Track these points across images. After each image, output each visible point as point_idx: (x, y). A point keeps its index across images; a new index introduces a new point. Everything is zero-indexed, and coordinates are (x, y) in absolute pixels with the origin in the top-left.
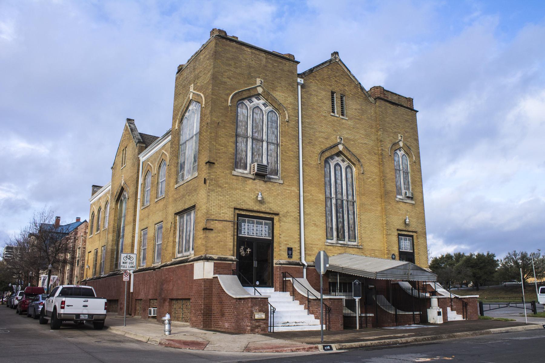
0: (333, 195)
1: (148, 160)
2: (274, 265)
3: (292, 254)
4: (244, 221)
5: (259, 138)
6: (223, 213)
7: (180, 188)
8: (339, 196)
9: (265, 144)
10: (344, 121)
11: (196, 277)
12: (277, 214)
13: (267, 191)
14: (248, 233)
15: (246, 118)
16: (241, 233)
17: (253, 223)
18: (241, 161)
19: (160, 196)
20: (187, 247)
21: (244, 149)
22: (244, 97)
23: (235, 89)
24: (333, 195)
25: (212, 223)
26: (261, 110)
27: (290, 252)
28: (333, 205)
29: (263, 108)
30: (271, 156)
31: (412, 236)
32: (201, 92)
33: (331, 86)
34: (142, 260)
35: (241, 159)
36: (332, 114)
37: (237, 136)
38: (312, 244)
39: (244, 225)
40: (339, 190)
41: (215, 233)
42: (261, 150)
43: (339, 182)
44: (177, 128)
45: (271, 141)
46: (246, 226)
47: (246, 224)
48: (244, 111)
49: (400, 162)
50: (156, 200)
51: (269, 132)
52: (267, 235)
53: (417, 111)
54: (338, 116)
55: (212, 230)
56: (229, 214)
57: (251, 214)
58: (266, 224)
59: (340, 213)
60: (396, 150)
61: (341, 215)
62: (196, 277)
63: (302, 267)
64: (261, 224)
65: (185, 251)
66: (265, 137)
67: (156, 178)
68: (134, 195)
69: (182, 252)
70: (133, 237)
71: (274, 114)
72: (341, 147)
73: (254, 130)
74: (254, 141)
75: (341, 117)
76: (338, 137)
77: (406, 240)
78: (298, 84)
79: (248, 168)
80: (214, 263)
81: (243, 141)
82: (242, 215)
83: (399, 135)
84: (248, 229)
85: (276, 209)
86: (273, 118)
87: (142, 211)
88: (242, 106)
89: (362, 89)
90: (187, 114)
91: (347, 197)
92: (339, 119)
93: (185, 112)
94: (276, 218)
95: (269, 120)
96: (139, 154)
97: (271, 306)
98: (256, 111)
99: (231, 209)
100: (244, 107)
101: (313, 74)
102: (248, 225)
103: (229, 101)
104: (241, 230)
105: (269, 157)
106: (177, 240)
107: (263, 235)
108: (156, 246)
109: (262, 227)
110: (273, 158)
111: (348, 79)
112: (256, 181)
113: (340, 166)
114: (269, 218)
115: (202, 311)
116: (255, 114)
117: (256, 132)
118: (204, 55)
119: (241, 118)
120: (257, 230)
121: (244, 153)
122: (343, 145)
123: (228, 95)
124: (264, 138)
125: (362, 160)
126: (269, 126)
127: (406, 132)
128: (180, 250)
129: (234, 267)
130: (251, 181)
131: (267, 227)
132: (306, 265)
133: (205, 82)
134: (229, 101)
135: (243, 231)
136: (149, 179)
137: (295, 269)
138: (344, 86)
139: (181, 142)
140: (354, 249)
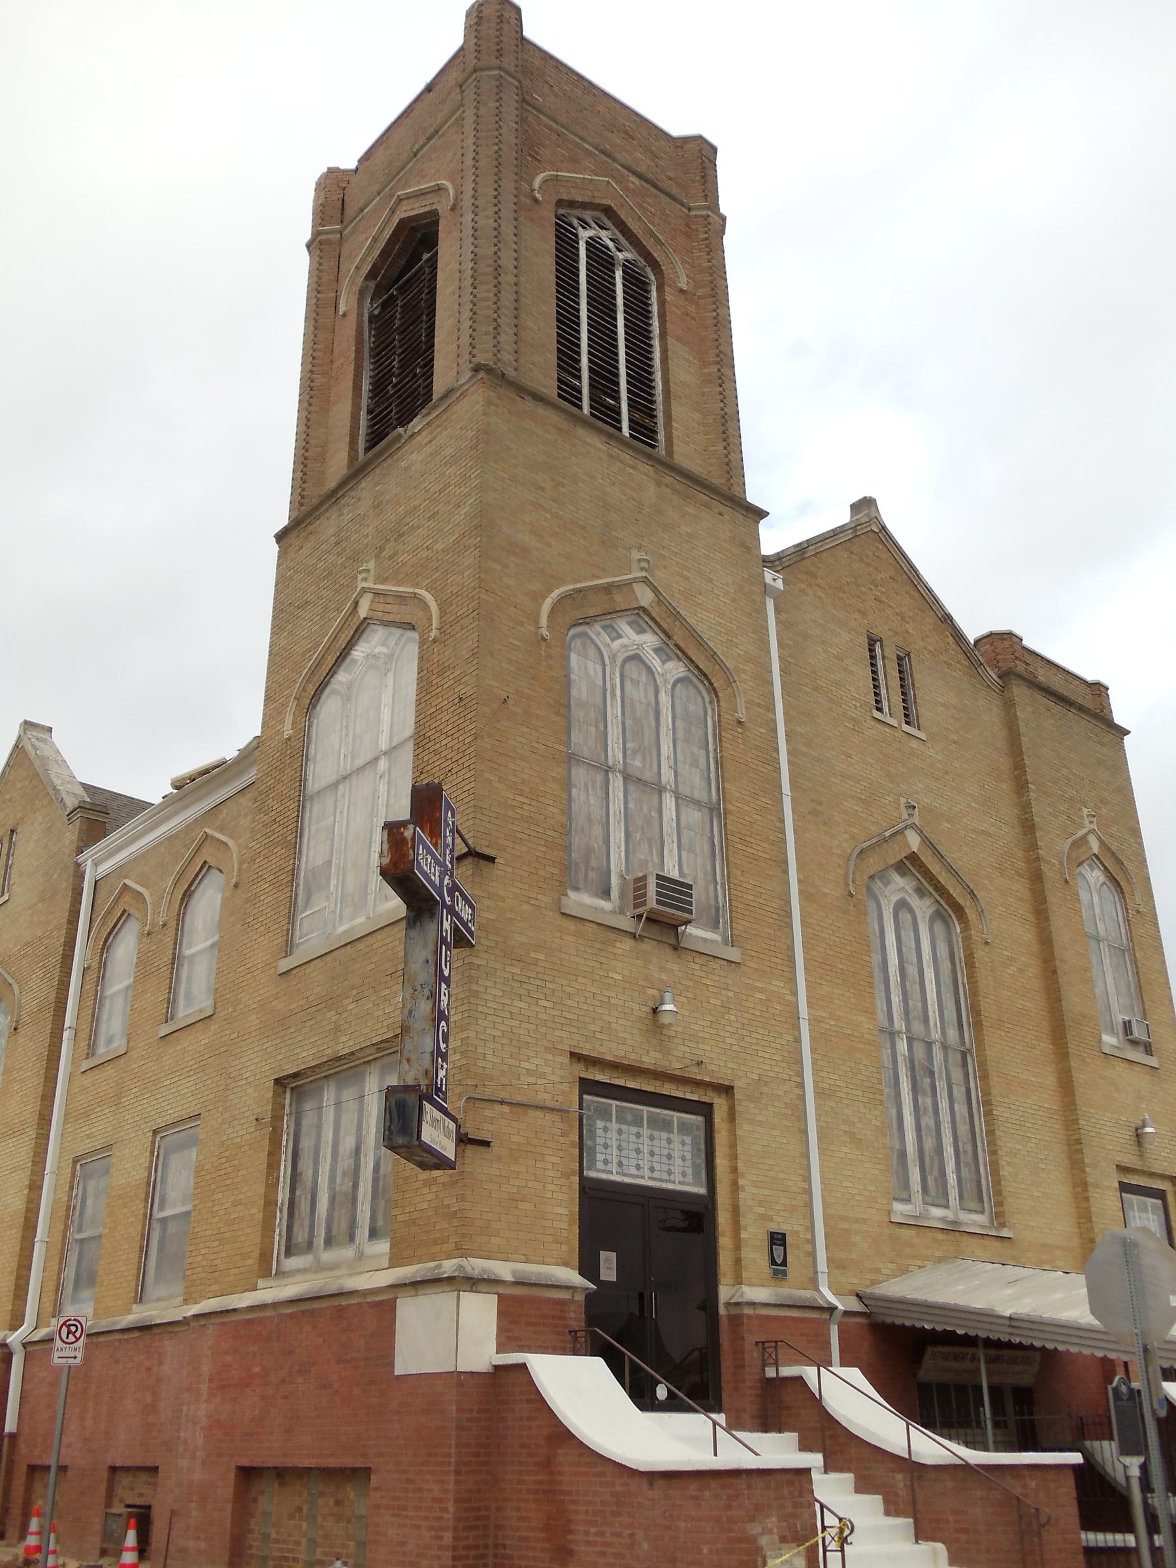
0: (899, 1024)
1: (122, 870)
2: (722, 1311)
3: (784, 1263)
4: (605, 1114)
5: (647, 776)
6: (529, 1072)
7: (309, 969)
8: (918, 1028)
9: (669, 801)
10: (914, 744)
11: (398, 1371)
12: (727, 1090)
13: (687, 989)
14: (620, 1164)
15: (599, 692)
16: (592, 1167)
17: (638, 1122)
18: (587, 860)
19: (185, 1013)
20: (342, 1225)
21: (598, 813)
22: (592, 612)
23: (563, 582)
24: (899, 1024)
25: (488, 1113)
26: (650, 671)
27: (778, 1251)
28: (900, 1059)
29: (655, 662)
30: (691, 850)
31: (1160, 1195)
32: (417, 585)
33: (864, 614)
34: (69, 1287)
35: (589, 851)
36: (877, 714)
37: (571, 759)
38: (845, 1219)
39: (606, 1129)
40: (915, 1003)
41: (499, 1159)
42: (656, 824)
43: (912, 970)
44: (288, 732)
45: (687, 792)
46: (613, 1135)
47: (614, 1126)
48: (593, 667)
49: (1097, 911)
50: (164, 1030)
51: (680, 757)
52: (690, 1179)
53: (1128, 732)
54: (894, 723)
55: (486, 1144)
56: (554, 1080)
57: (620, 1082)
58: (684, 1128)
59: (924, 1093)
60: (1080, 864)
61: (929, 1100)
62: (398, 1371)
63: (826, 1316)
64: (666, 1126)
65: (329, 1242)
66: (667, 776)
67: (168, 940)
68: (49, 1015)
69: (310, 1246)
70: (35, 1187)
71: (692, 690)
72: (914, 841)
73: (629, 745)
74: (631, 788)
75: (906, 728)
76: (903, 800)
77: (1143, 1209)
78: (766, 589)
79: (615, 894)
80: (501, 1298)
81: (594, 782)
82: (607, 1085)
83: (1085, 811)
84: (620, 1148)
85: (719, 1068)
86: (692, 707)
87: (87, 1081)
88: (584, 645)
89: (958, 635)
90: (342, 677)
91: (944, 1033)
92: (898, 734)
93: (332, 672)
94: (720, 1105)
95: (679, 711)
96: (80, 851)
97: (822, 1507)
98: (633, 670)
99: (559, 1059)
100: (592, 652)
101: (807, 563)
102: (620, 1132)
103: (544, 621)
104: (593, 1153)
105: (684, 854)
106: (283, 1196)
107: (678, 1177)
108: (157, 1227)
109: (669, 1141)
110: (699, 860)
111: (912, 597)
112: (647, 946)
113: (911, 911)
114: (697, 1102)
115: (448, 1536)
116: (628, 684)
117: (635, 753)
118: (428, 450)
119: (580, 690)
120: (638, 1151)
121: (598, 831)
122: (921, 833)
123: (539, 598)
124: (664, 780)
125: (980, 894)
126: (680, 735)
127: (1105, 802)
128: (300, 1236)
129: (576, 1318)
130: (627, 944)
131: (688, 1140)
132: (841, 1307)
133: (439, 546)
134: (544, 621)
135: (600, 1157)
136: (126, 948)
137: (806, 1329)
138: (903, 619)
139: (313, 786)
140: (986, 1242)
